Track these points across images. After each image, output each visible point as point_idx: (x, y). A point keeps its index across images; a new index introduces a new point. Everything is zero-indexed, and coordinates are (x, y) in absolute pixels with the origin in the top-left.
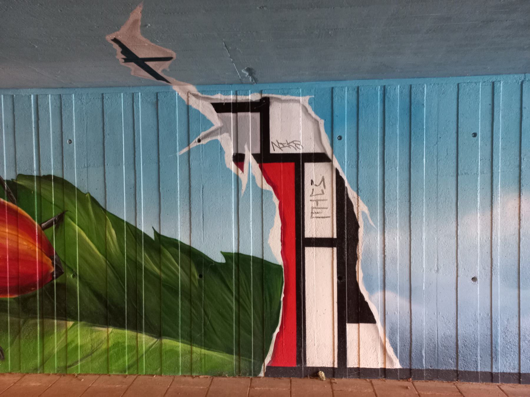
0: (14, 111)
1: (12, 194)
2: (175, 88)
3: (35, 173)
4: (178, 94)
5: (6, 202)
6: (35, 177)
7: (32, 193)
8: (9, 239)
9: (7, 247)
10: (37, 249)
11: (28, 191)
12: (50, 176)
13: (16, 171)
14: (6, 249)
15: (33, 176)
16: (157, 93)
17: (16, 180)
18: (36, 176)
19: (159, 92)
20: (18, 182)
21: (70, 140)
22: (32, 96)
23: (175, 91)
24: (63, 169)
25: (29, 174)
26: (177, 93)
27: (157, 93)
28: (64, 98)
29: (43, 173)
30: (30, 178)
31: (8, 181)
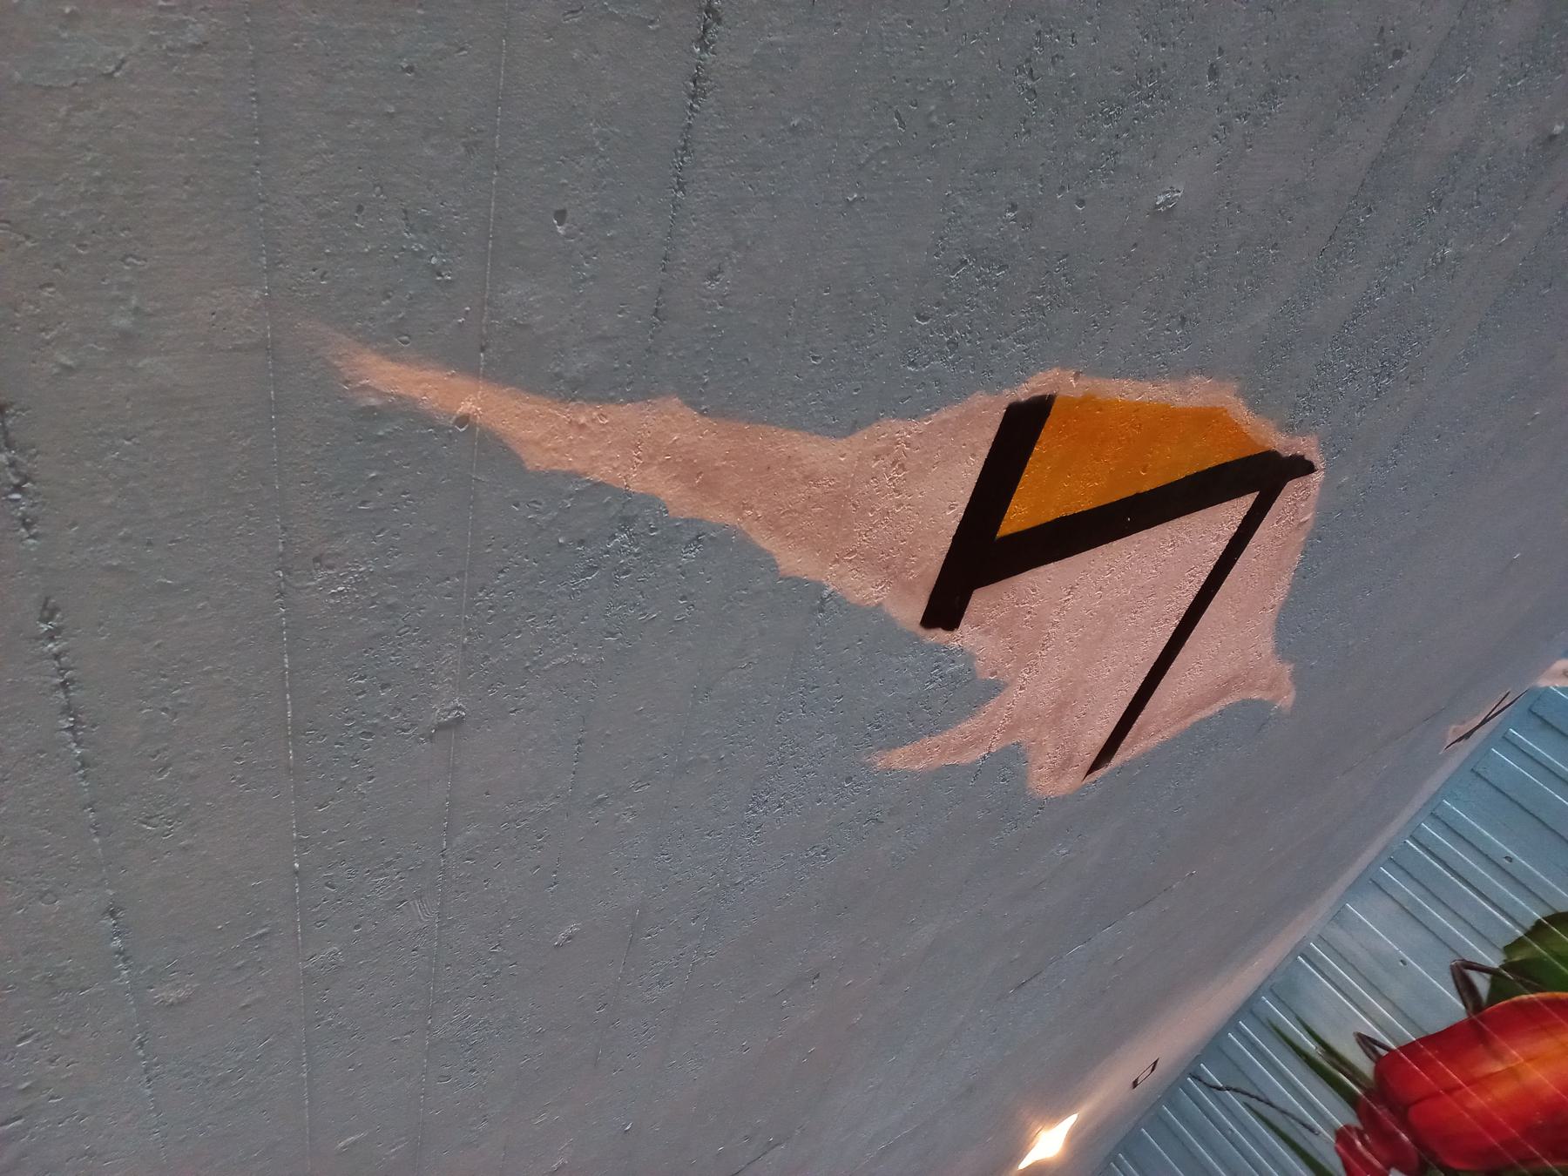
0: (1439, 899)
1: (1527, 981)
2: (1543, 683)
3: (1520, 933)
4: (1556, 687)
5: (1532, 996)
6: (1526, 938)
7: (451, 281)
8: (1460, 1087)
9: (1496, 1144)
10: (1551, 1165)
11: (1538, 962)
12: (1539, 923)
13: (1495, 946)
14: (1495, 1147)
15: (1520, 938)
16: (1530, 710)
17: (1510, 957)
18: (1525, 935)
19: (1531, 706)
20: (1517, 959)
21: (1506, 858)
22: (1408, 841)
23: (1547, 688)
24: (1543, 901)
25: (1513, 939)
26: (1551, 687)
27: (1530, 710)
28: (1438, 813)
29: (1529, 925)
30: (1519, 943)
31: (1502, 967)
